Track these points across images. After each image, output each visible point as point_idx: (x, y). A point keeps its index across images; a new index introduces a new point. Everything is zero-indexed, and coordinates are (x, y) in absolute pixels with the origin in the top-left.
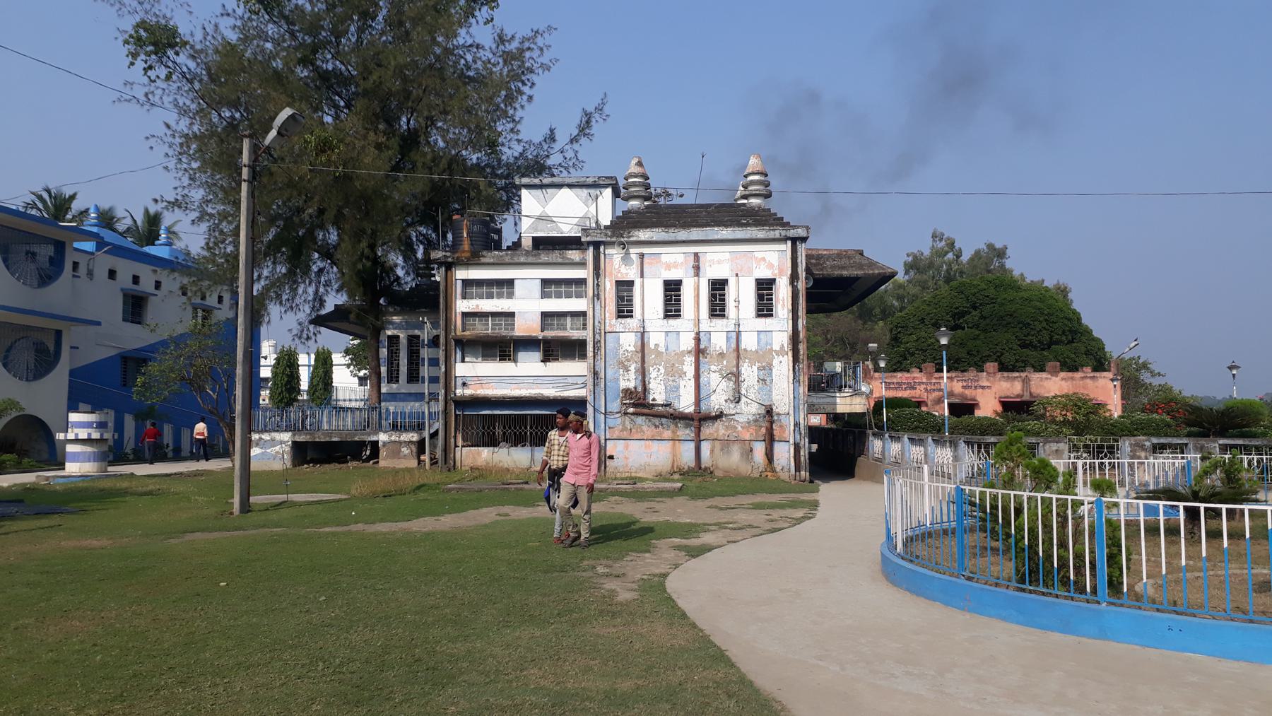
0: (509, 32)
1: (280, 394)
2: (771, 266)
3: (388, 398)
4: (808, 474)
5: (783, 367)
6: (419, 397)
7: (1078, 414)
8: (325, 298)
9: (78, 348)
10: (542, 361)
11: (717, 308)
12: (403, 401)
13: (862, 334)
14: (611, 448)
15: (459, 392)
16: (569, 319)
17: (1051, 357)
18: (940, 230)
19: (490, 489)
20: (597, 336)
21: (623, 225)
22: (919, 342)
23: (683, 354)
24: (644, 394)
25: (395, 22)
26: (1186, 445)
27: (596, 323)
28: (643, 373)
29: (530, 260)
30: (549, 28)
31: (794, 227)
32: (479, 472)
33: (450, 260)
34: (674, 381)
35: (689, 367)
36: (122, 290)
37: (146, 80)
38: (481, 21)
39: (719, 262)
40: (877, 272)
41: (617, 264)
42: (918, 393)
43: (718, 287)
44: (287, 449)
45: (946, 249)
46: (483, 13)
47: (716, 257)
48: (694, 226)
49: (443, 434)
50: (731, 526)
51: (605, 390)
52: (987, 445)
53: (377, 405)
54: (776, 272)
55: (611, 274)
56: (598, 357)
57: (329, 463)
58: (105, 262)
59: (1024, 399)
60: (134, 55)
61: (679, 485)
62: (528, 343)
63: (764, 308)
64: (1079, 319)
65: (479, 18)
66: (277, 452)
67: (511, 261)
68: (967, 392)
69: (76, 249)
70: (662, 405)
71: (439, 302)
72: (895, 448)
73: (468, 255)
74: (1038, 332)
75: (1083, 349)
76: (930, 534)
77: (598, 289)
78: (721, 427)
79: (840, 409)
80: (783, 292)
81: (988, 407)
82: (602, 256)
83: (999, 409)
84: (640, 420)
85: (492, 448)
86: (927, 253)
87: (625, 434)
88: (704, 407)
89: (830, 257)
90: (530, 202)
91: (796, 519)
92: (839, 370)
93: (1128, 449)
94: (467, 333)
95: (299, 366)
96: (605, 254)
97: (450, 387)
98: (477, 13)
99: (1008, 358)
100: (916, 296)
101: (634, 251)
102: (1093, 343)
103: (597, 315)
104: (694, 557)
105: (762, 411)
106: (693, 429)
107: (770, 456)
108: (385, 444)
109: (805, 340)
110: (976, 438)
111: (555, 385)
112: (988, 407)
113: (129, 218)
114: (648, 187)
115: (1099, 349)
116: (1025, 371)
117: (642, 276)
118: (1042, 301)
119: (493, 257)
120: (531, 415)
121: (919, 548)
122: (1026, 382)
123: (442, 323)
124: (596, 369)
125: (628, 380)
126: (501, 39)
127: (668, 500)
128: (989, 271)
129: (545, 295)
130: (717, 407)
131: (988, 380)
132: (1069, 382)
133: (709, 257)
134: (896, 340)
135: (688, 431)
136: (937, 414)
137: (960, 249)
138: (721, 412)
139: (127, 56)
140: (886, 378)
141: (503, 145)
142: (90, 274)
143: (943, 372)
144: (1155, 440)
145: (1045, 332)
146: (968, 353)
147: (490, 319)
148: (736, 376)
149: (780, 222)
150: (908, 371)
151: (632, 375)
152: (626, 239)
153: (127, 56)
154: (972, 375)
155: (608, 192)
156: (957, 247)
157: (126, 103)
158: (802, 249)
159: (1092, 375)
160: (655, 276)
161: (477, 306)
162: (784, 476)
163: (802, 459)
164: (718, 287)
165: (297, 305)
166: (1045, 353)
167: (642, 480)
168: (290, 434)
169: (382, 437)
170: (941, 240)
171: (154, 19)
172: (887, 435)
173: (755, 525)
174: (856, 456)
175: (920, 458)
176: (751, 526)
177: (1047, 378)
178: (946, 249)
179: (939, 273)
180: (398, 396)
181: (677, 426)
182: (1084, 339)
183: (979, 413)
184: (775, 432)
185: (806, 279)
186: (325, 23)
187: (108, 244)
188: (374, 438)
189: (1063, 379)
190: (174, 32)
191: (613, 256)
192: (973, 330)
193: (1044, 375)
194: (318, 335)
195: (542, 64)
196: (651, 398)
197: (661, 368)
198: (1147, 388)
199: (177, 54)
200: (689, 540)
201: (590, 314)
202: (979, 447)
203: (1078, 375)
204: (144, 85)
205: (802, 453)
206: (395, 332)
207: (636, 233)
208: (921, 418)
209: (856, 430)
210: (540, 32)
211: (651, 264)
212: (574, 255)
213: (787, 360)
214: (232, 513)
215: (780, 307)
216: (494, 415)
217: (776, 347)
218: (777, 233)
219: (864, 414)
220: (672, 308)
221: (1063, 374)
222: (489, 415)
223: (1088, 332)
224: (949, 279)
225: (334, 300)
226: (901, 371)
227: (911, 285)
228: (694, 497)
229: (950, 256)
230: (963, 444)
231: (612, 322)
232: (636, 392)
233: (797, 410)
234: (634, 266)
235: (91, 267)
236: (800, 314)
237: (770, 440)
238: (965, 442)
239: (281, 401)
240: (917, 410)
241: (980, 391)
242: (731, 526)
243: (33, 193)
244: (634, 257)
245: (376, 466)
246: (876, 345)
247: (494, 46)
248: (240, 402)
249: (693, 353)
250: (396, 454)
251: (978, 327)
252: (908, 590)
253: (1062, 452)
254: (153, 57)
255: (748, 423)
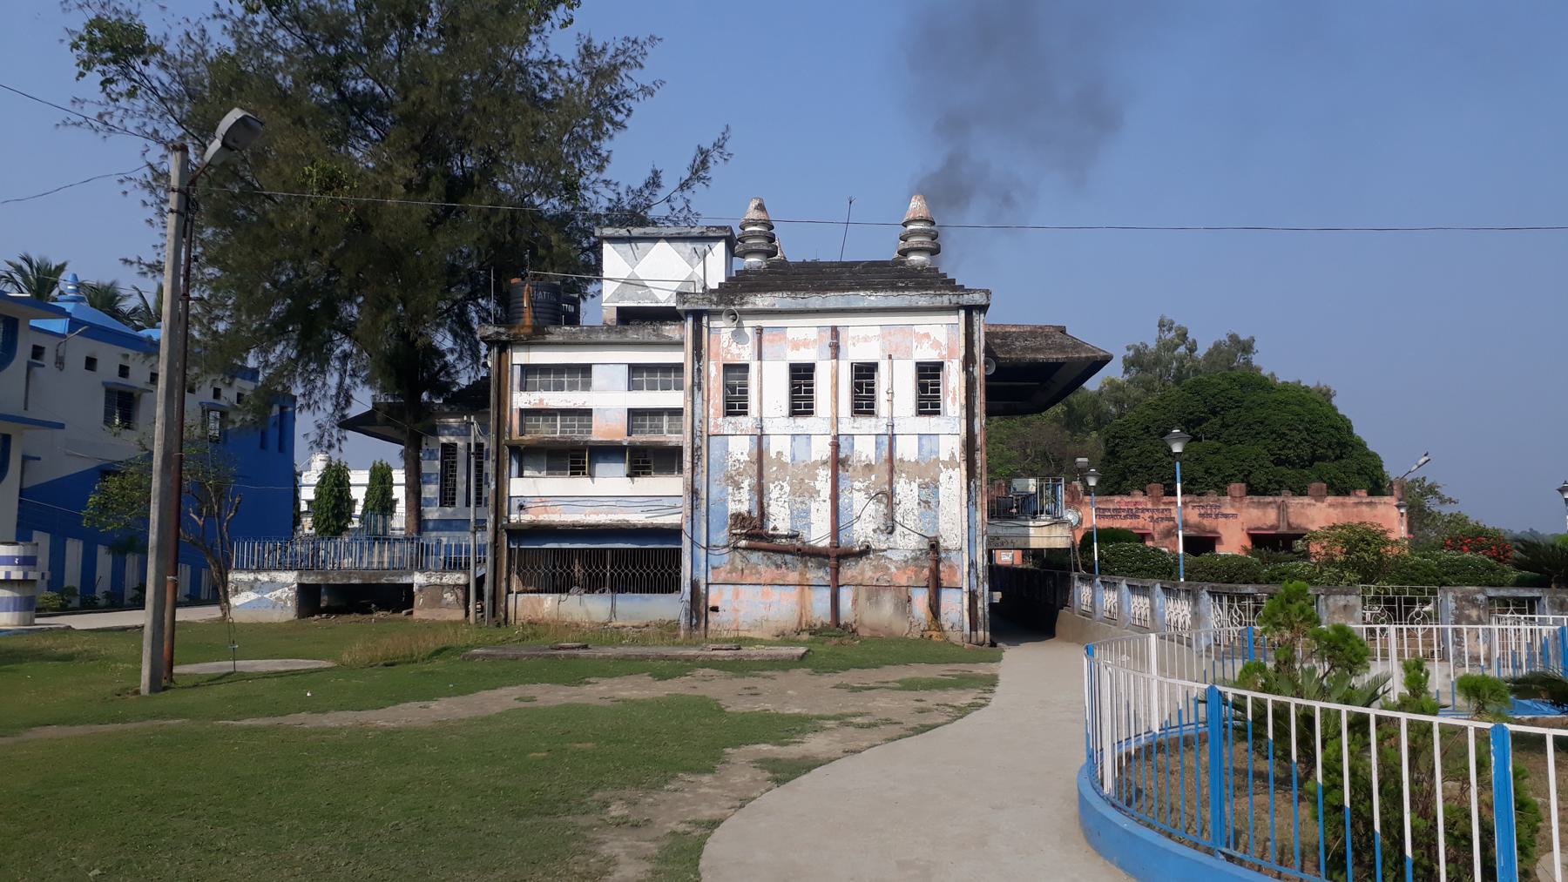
0: (598, 44)
1: (325, 521)
2: (936, 345)
3: (441, 526)
4: (988, 634)
5: (953, 483)
6: (462, 525)
7: (1366, 551)
8: (352, 392)
9: (39, 459)
10: (628, 476)
11: (864, 403)
12: (460, 530)
13: (1070, 448)
14: (715, 596)
15: (514, 518)
16: (666, 418)
17: (1313, 476)
18: (1169, 317)
19: (530, 657)
20: (697, 441)
21: (738, 286)
22: (1143, 456)
23: (815, 465)
24: (762, 520)
25: (449, 30)
26: (1539, 599)
27: (697, 423)
28: (760, 491)
29: (614, 338)
30: (652, 38)
31: (969, 291)
32: (535, 627)
33: (504, 338)
34: (802, 502)
35: (823, 484)
36: (104, 383)
37: (102, 97)
38: (557, 23)
39: (866, 339)
40: (1083, 355)
41: (726, 342)
42: (1142, 523)
43: (864, 374)
44: (292, 594)
45: (1177, 341)
46: (560, 12)
47: (862, 332)
48: (831, 290)
49: (492, 574)
50: (859, 720)
51: (708, 515)
52: (1242, 597)
53: (415, 535)
54: (944, 353)
55: (717, 355)
56: (698, 470)
57: (350, 612)
58: (81, 347)
59: (1281, 531)
60: (88, 65)
61: (802, 650)
62: (609, 451)
63: (928, 403)
64: (1349, 428)
65: (554, 20)
66: (278, 599)
67: (586, 340)
68: (1206, 522)
69: (33, 328)
70: (786, 537)
71: (489, 395)
72: (1109, 598)
73: (528, 331)
74: (1297, 444)
75: (1355, 467)
76: (1160, 747)
77: (699, 375)
78: (867, 567)
79: (1034, 543)
80: (953, 381)
81: (1232, 543)
82: (705, 330)
83: (1248, 544)
84: (755, 557)
85: (557, 595)
86: (1152, 345)
87: (735, 577)
88: (843, 539)
89: (1020, 335)
90: (614, 260)
91: (959, 709)
92: (1032, 489)
93: (1452, 605)
94: (527, 437)
95: (350, 485)
96: (709, 328)
97: (502, 511)
98: (552, 13)
99: (1259, 477)
100: (1138, 400)
101: (749, 324)
102: (1368, 459)
103: (698, 411)
104: (779, 782)
105: (925, 545)
106: (828, 570)
107: (935, 608)
108: (421, 588)
109: (984, 447)
110: (1225, 587)
111: (645, 509)
112: (1232, 543)
113: (136, 294)
114: (771, 239)
115: (1376, 467)
116: (1280, 494)
117: (760, 358)
118: (1301, 404)
119: (563, 335)
120: (612, 549)
121: (1143, 776)
122: (1282, 508)
123: (492, 423)
124: (696, 486)
125: (740, 501)
126: (588, 52)
127: (779, 674)
128: (1232, 369)
129: (633, 386)
130: (862, 539)
131: (1233, 506)
132: (1339, 510)
133: (852, 332)
134: (1112, 454)
135: (821, 573)
136: (1166, 550)
137: (1195, 341)
138: (868, 547)
139: (78, 65)
140: (1100, 503)
141: (585, 188)
142: (60, 362)
143: (1176, 495)
144: (1492, 592)
145: (1305, 444)
146: (1206, 472)
147: (559, 418)
148: (888, 497)
149: (951, 285)
150: (1129, 494)
151: (745, 494)
152: (737, 307)
153: (78, 65)
154: (1212, 499)
155: (720, 248)
156: (1190, 339)
157: (74, 127)
158: (980, 322)
159: (1368, 500)
160: (777, 358)
161: (541, 401)
162: (955, 637)
163: (980, 613)
164: (864, 374)
165: (316, 402)
166: (1306, 472)
167: (752, 641)
168: (296, 573)
169: (418, 579)
170: (1170, 330)
171: (114, 17)
172: (1098, 580)
173: (896, 719)
174: (1058, 604)
175: (1143, 613)
176: (888, 722)
177: (1309, 504)
178: (1177, 341)
179: (1168, 370)
180: (454, 524)
181: (806, 566)
182: (1355, 454)
183: (1221, 550)
184: (942, 575)
185: (986, 363)
186: (355, 28)
187: (83, 323)
188: (406, 580)
189: (1330, 505)
190: (141, 33)
191: (721, 333)
192: (1212, 442)
193: (1306, 500)
194: (343, 442)
195: (643, 86)
196: (771, 526)
197: (785, 484)
198: (1434, 518)
199: (146, 63)
200: (785, 749)
201: (688, 411)
202: (1231, 599)
203: (1351, 500)
204: (100, 104)
205: (980, 605)
206: (452, 439)
207: (752, 299)
208: (1146, 556)
209: (1058, 572)
210: (639, 41)
211: (772, 341)
212: (671, 331)
213: (959, 474)
214: (137, 692)
215: (949, 401)
216: (561, 549)
217: (944, 456)
218: (945, 300)
219: (1065, 551)
220: (801, 403)
221: (1330, 499)
222: (555, 549)
223: (1361, 445)
224: (1178, 380)
225: (363, 400)
226: (1120, 494)
227: (1131, 386)
228: (820, 669)
229: (1182, 350)
230: (1207, 596)
231: (718, 421)
232: (752, 519)
233: (972, 543)
234: (750, 344)
235: (61, 354)
236: (977, 410)
237: (936, 585)
238: (1209, 592)
239: (326, 530)
240: (1140, 545)
241: (1222, 520)
242: (859, 720)
243: (10, 264)
244: (748, 331)
245: (409, 617)
246: (1086, 460)
247: (578, 61)
248: (156, 530)
249: (829, 464)
250: (436, 601)
251: (1219, 438)
252: (1121, 866)
253: (1354, 607)
254: (113, 67)
255: (906, 562)
